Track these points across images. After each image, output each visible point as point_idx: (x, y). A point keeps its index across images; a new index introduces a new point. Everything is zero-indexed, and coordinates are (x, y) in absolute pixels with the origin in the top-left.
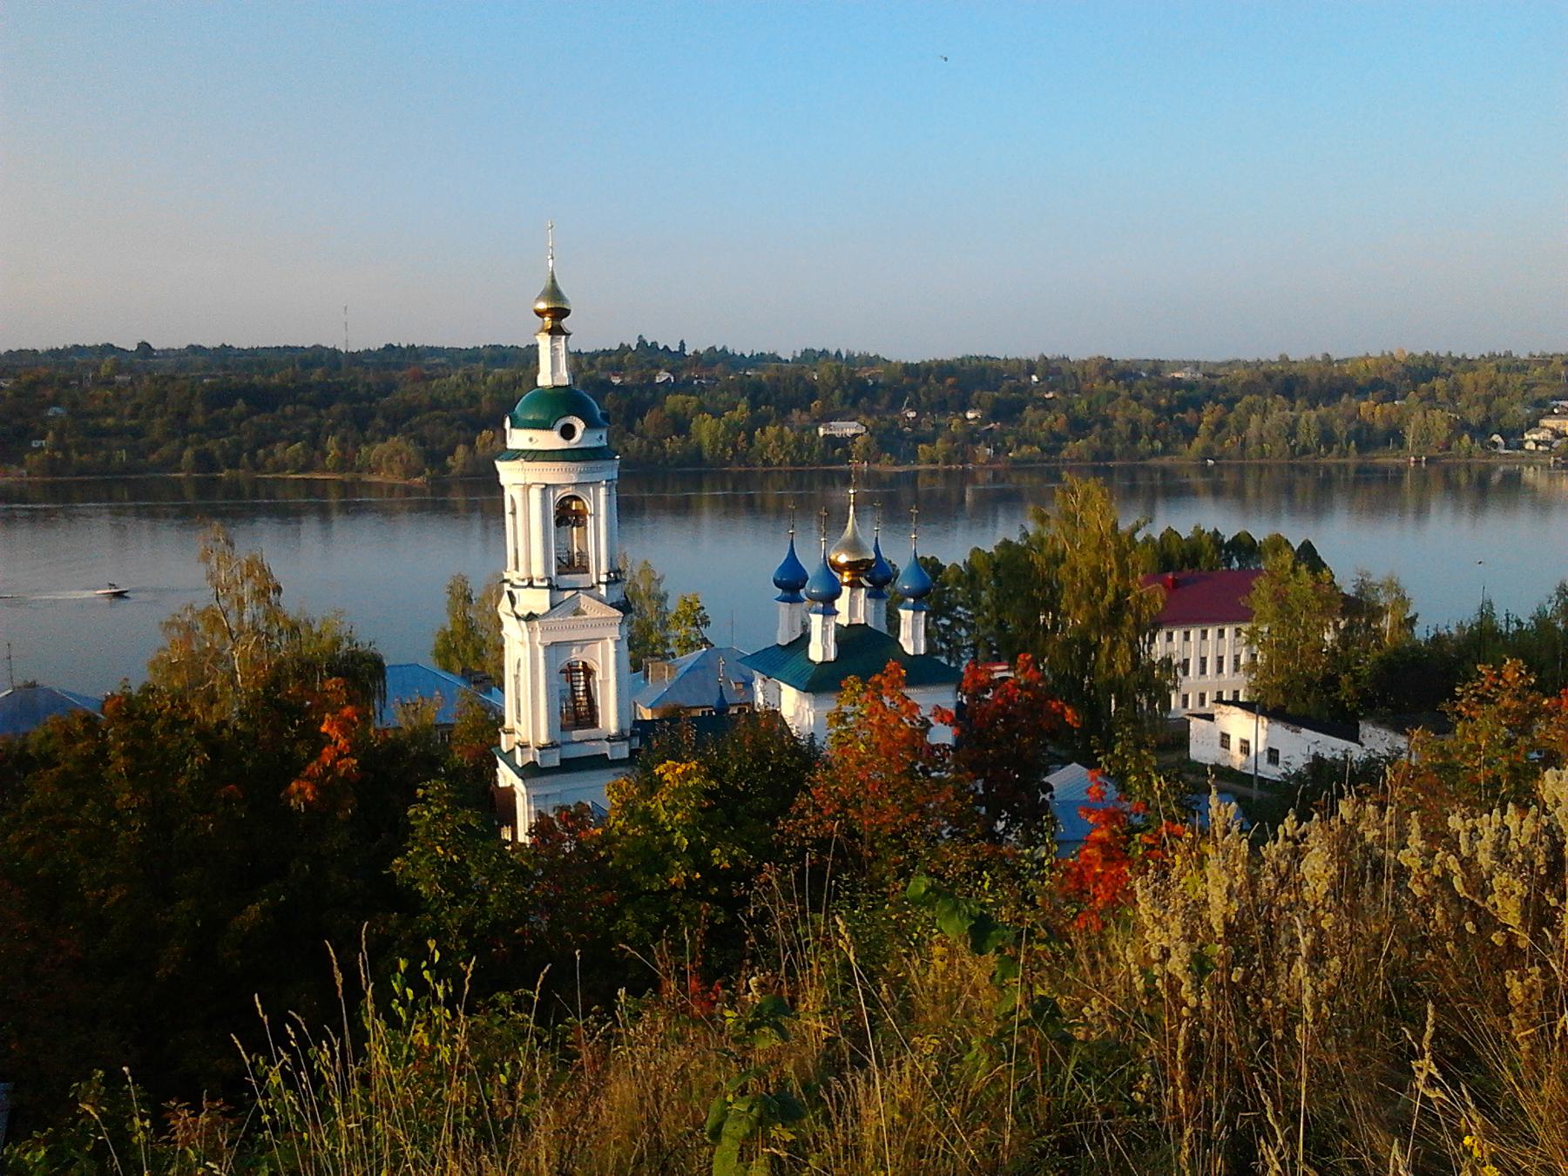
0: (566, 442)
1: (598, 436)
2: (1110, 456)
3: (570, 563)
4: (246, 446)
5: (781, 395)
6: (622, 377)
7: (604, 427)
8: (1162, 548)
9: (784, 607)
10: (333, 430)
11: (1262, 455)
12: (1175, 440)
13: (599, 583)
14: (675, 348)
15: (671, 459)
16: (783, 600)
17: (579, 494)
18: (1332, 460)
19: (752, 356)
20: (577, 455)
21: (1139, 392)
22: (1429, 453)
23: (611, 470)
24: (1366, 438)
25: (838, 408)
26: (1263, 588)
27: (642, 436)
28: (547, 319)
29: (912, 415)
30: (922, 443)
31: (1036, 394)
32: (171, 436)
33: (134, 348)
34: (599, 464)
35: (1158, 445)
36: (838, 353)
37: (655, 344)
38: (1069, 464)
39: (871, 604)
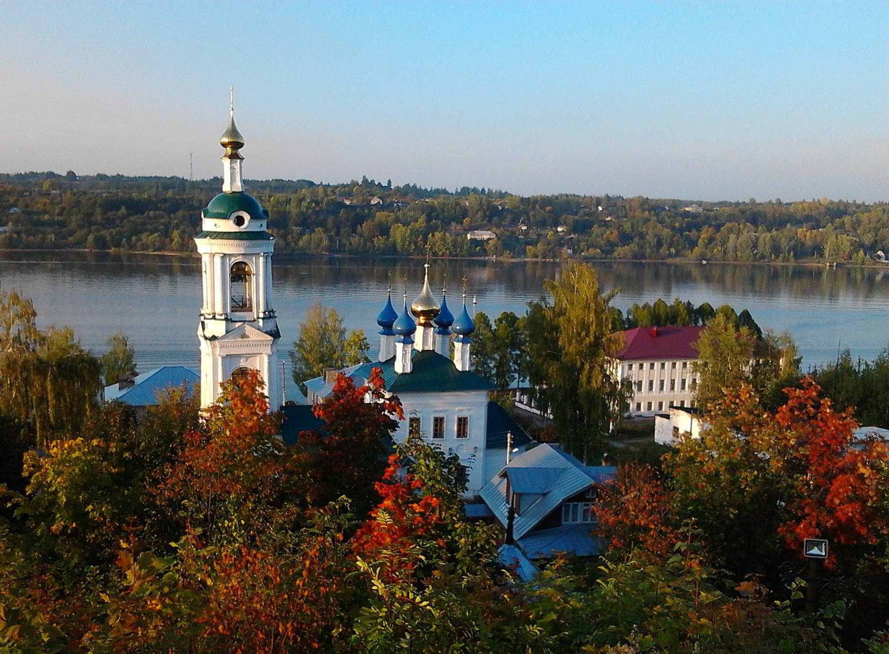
0: (238, 227)
1: (259, 225)
2: (643, 256)
3: (241, 305)
4: (126, 234)
5: (446, 214)
6: (351, 200)
7: (264, 219)
8: (654, 310)
9: (383, 338)
10: (177, 226)
11: (736, 259)
12: (684, 248)
13: (258, 318)
14: (385, 184)
15: (378, 250)
16: (383, 334)
17: (245, 261)
18: (779, 263)
19: (431, 190)
20: (244, 236)
21: (663, 219)
22: (839, 261)
23: (269, 247)
24: (800, 251)
25: (479, 222)
26: (705, 337)
27: (361, 236)
28: (229, 149)
29: (524, 228)
30: (529, 245)
31: (600, 218)
32: (81, 227)
33: (64, 174)
34: (259, 242)
35: (673, 250)
36: (483, 190)
37: (373, 181)
38: (618, 260)
39: (439, 338)
